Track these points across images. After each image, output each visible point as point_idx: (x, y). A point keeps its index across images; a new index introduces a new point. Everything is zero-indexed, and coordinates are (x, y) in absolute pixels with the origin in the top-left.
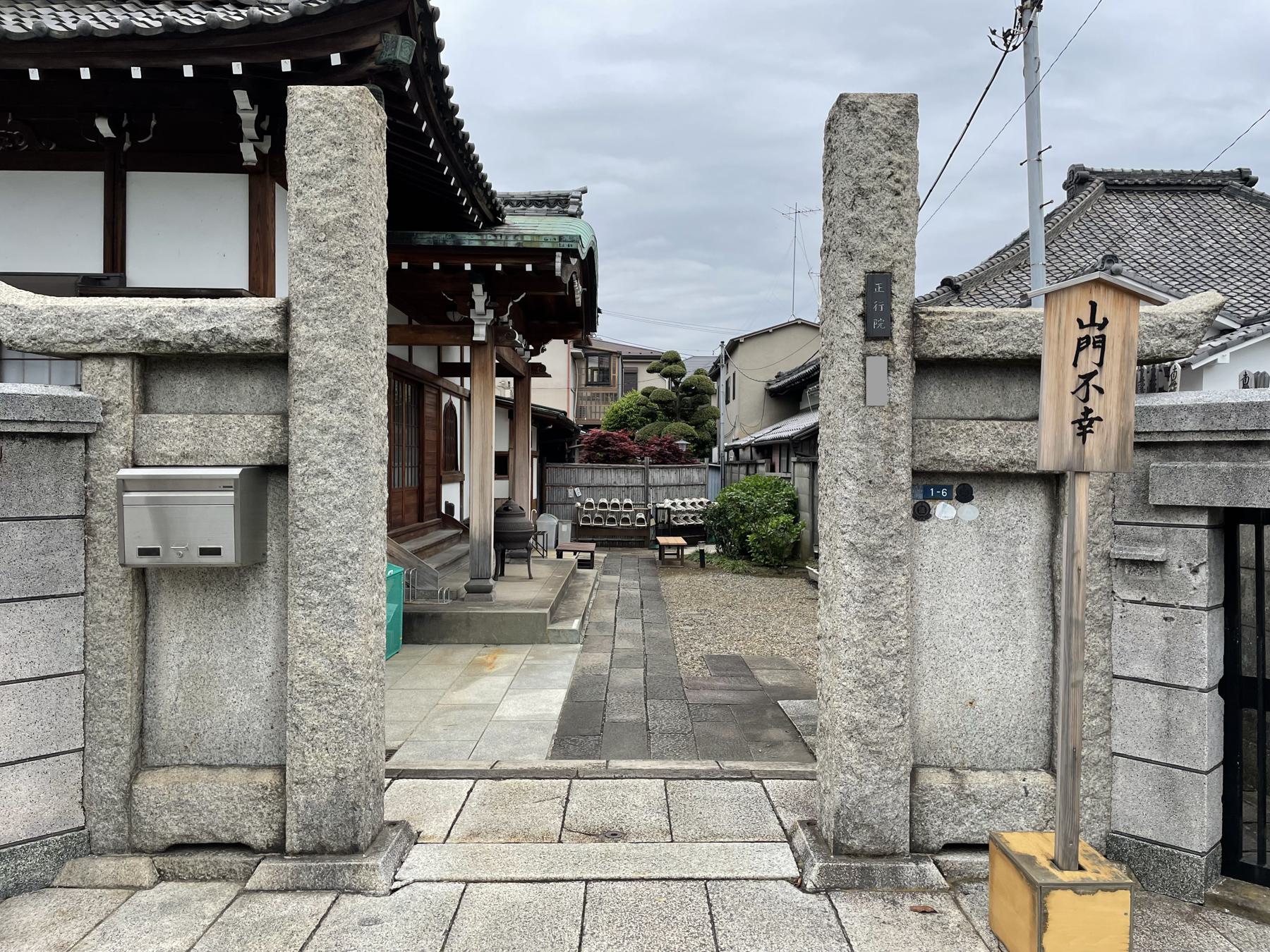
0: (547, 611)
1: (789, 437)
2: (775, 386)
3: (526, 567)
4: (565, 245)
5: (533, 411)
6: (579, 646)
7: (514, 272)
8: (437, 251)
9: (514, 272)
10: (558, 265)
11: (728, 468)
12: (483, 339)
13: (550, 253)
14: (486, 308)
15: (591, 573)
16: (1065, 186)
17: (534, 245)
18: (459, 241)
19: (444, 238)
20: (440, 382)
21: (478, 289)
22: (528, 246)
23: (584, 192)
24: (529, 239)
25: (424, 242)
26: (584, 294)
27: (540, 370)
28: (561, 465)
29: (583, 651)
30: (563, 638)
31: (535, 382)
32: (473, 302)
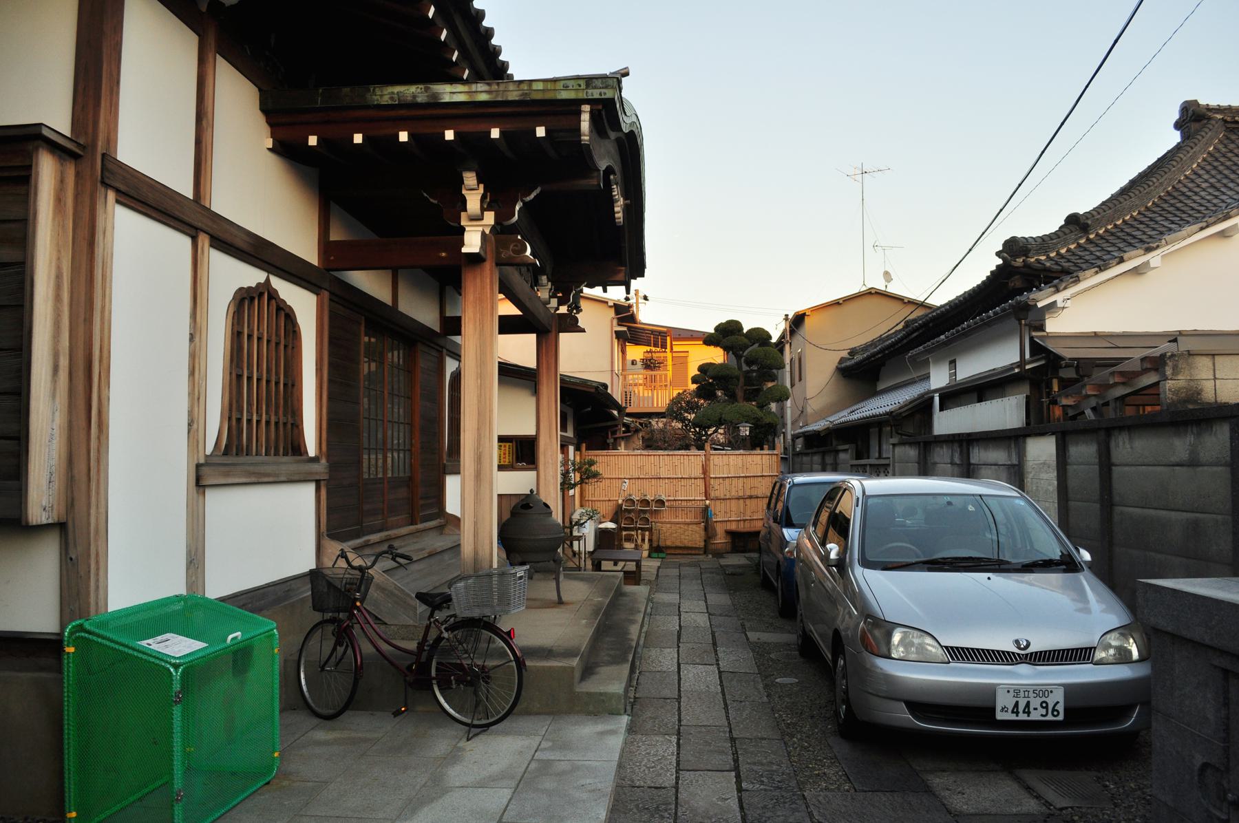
0: (575, 662)
1: (887, 413)
2: (848, 363)
3: (554, 584)
4: (595, 94)
5: (562, 380)
6: (625, 719)
7: (518, 139)
8: (406, 113)
9: (518, 139)
10: (585, 125)
11: (798, 460)
12: (476, 250)
13: (572, 107)
14: (483, 210)
15: (641, 591)
16: (1178, 126)
17: (549, 96)
18: (435, 96)
19: (412, 91)
20: (441, 342)
21: (470, 179)
22: (539, 96)
23: (627, 74)
24: (540, 86)
25: (385, 100)
26: (627, 209)
27: (570, 324)
28: (604, 452)
29: (631, 730)
30: (599, 707)
31: (564, 338)
32: (464, 201)
